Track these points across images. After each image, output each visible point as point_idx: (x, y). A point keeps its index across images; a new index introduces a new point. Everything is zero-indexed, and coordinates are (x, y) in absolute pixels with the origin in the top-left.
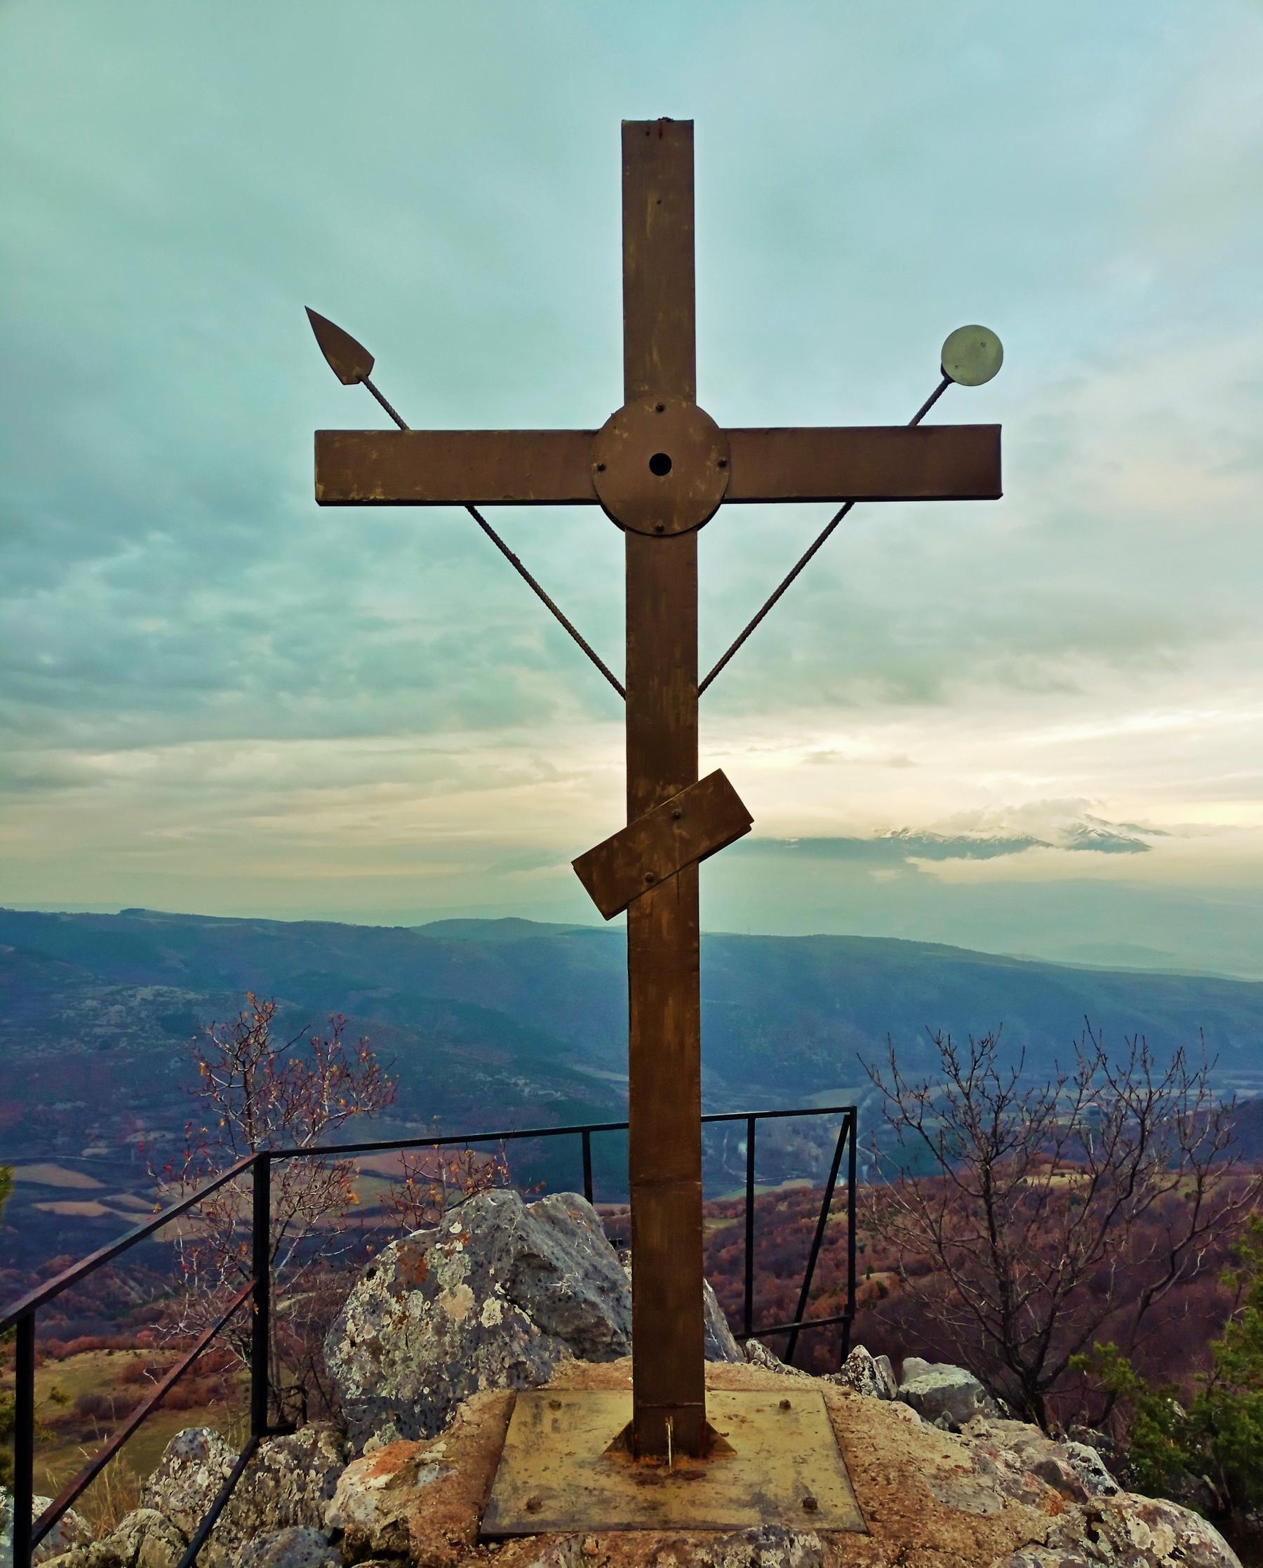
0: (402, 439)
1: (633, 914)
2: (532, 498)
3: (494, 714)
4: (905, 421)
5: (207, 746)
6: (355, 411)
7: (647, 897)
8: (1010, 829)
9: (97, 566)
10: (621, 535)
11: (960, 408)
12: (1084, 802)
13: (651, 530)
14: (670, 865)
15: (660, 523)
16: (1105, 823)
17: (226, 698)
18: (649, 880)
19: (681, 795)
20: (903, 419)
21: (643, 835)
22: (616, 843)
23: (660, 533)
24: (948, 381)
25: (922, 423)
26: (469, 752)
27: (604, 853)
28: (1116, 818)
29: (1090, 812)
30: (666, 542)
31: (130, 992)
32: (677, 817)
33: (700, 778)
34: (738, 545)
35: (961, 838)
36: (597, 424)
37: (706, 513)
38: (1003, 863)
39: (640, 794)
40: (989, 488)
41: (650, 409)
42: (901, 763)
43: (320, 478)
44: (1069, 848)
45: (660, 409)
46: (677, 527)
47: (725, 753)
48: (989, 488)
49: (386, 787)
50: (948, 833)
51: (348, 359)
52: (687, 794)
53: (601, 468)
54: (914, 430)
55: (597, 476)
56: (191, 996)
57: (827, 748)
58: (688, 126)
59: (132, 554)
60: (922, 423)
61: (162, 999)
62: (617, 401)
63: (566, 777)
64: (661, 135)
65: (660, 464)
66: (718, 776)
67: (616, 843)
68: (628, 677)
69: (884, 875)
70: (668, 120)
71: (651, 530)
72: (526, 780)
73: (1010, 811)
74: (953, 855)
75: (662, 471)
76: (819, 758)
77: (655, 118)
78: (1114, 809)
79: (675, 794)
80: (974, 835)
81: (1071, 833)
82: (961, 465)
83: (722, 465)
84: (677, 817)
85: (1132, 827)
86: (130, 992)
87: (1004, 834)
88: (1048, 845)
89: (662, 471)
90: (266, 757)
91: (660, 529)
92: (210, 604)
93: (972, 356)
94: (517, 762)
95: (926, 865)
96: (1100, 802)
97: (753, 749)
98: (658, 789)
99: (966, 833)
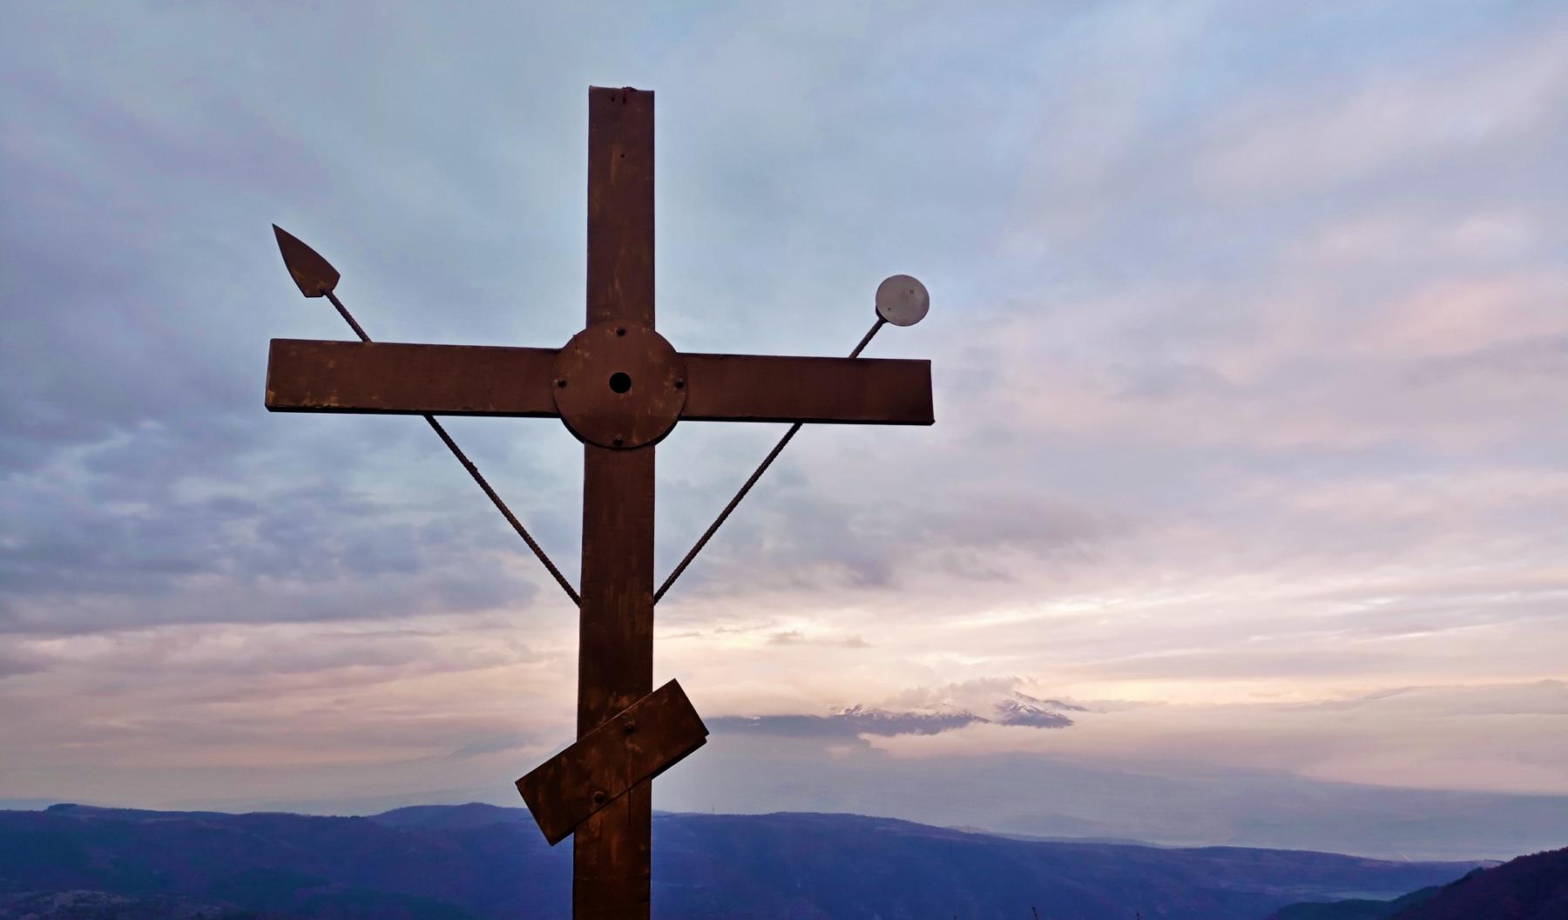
0: (364, 353)
1: (581, 838)
2: (492, 409)
3: (475, 597)
4: (846, 354)
5: (169, 631)
6: (316, 322)
7: (596, 819)
8: (950, 706)
9: (81, 451)
10: (582, 446)
11: (893, 345)
12: (1017, 680)
13: (610, 443)
14: (622, 783)
15: (619, 437)
16: (1033, 700)
17: (199, 580)
18: (599, 799)
19: (635, 706)
20: (845, 353)
21: (594, 751)
22: (564, 759)
23: (619, 446)
24: (882, 321)
25: (860, 356)
26: (444, 633)
27: (551, 771)
28: (1042, 696)
29: (1023, 691)
30: (625, 455)
31: (47, 898)
32: (630, 731)
33: (655, 689)
34: (694, 461)
35: (908, 714)
36: (559, 344)
37: (663, 429)
38: (948, 738)
39: (592, 707)
40: (922, 414)
41: (611, 333)
42: (855, 643)
43: (271, 385)
44: (1005, 723)
45: (621, 333)
46: (636, 441)
47: (696, 634)
48: (922, 414)
49: (356, 670)
50: (896, 710)
51: (313, 274)
52: (641, 706)
53: (562, 384)
54: (853, 361)
55: (557, 391)
56: (117, 899)
57: (789, 630)
58: (649, 97)
59: (120, 440)
60: (860, 356)
61: (81, 905)
62: (580, 325)
63: (539, 658)
64: (625, 101)
65: (620, 383)
66: (673, 686)
67: (564, 759)
68: (582, 585)
69: (839, 751)
70: (632, 90)
71: (610, 443)
72: (501, 661)
73: (953, 688)
74: (904, 731)
75: (622, 389)
76: (782, 639)
77: (619, 86)
78: (1043, 685)
79: (629, 706)
80: (920, 711)
81: (1003, 709)
82: (899, 394)
83: (679, 385)
84: (630, 731)
85: (1056, 703)
86: (47, 898)
87: (946, 711)
88: (986, 721)
89: (622, 389)
90: (232, 640)
91: (621, 442)
92: (195, 489)
93: (902, 301)
94: (491, 644)
95: (877, 741)
96: (1031, 680)
97: (721, 631)
98: (611, 700)
99: (912, 710)
